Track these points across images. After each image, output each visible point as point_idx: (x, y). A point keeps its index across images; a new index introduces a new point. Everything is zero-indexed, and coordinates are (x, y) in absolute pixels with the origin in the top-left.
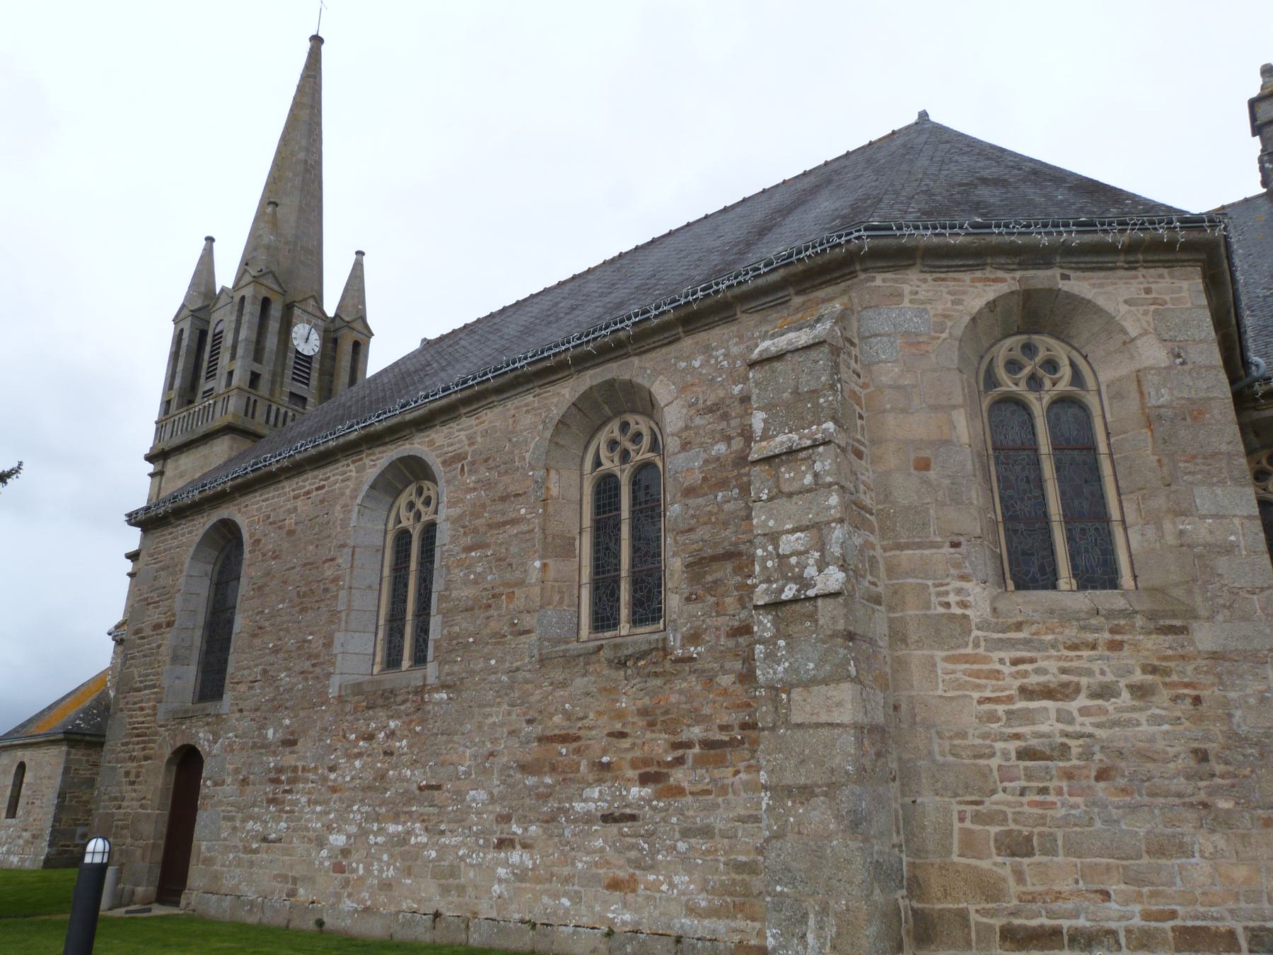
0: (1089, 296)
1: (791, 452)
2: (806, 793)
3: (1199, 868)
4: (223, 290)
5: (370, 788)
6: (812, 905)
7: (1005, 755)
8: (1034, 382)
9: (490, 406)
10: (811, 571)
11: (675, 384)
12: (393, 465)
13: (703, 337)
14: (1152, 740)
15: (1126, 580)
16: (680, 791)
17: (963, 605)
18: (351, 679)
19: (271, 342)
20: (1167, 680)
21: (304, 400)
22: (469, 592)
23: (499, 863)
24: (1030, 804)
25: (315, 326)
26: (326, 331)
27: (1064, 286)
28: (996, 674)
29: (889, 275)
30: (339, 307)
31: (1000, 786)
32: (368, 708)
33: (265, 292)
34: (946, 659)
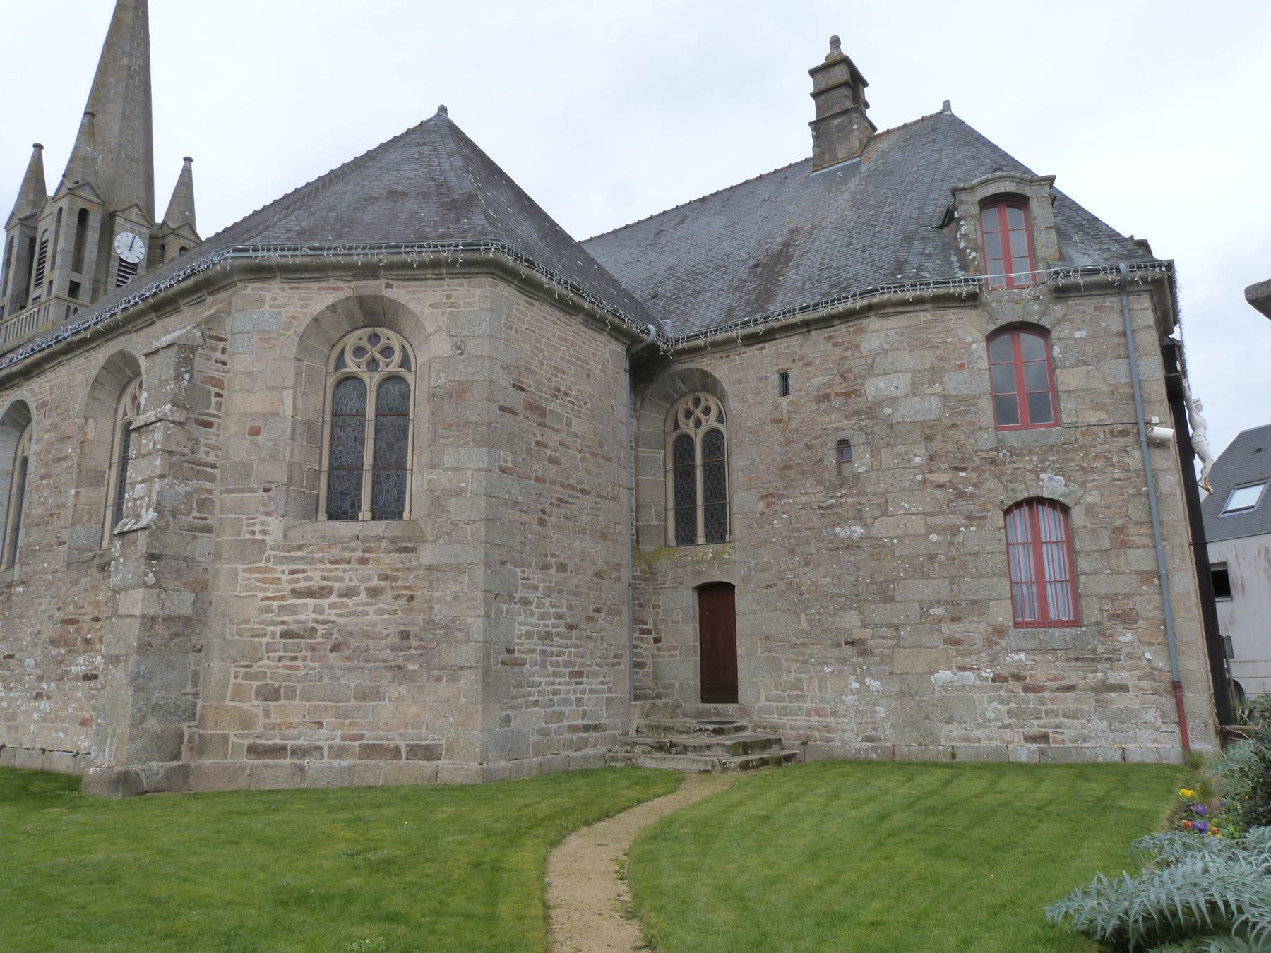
0: (403, 302)
7: (273, 635)
9: (60, 364)
14: (374, 625)
15: (406, 515)
17: (264, 533)
19: (91, 251)
20: (394, 584)
24: (285, 667)
25: (140, 235)
26: (152, 238)
27: (387, 293)
28: (277, 581)
29: (258, 285)
30: (167, 214)
31: (266, 655)
33: (81, 204)
34: (245, 570)
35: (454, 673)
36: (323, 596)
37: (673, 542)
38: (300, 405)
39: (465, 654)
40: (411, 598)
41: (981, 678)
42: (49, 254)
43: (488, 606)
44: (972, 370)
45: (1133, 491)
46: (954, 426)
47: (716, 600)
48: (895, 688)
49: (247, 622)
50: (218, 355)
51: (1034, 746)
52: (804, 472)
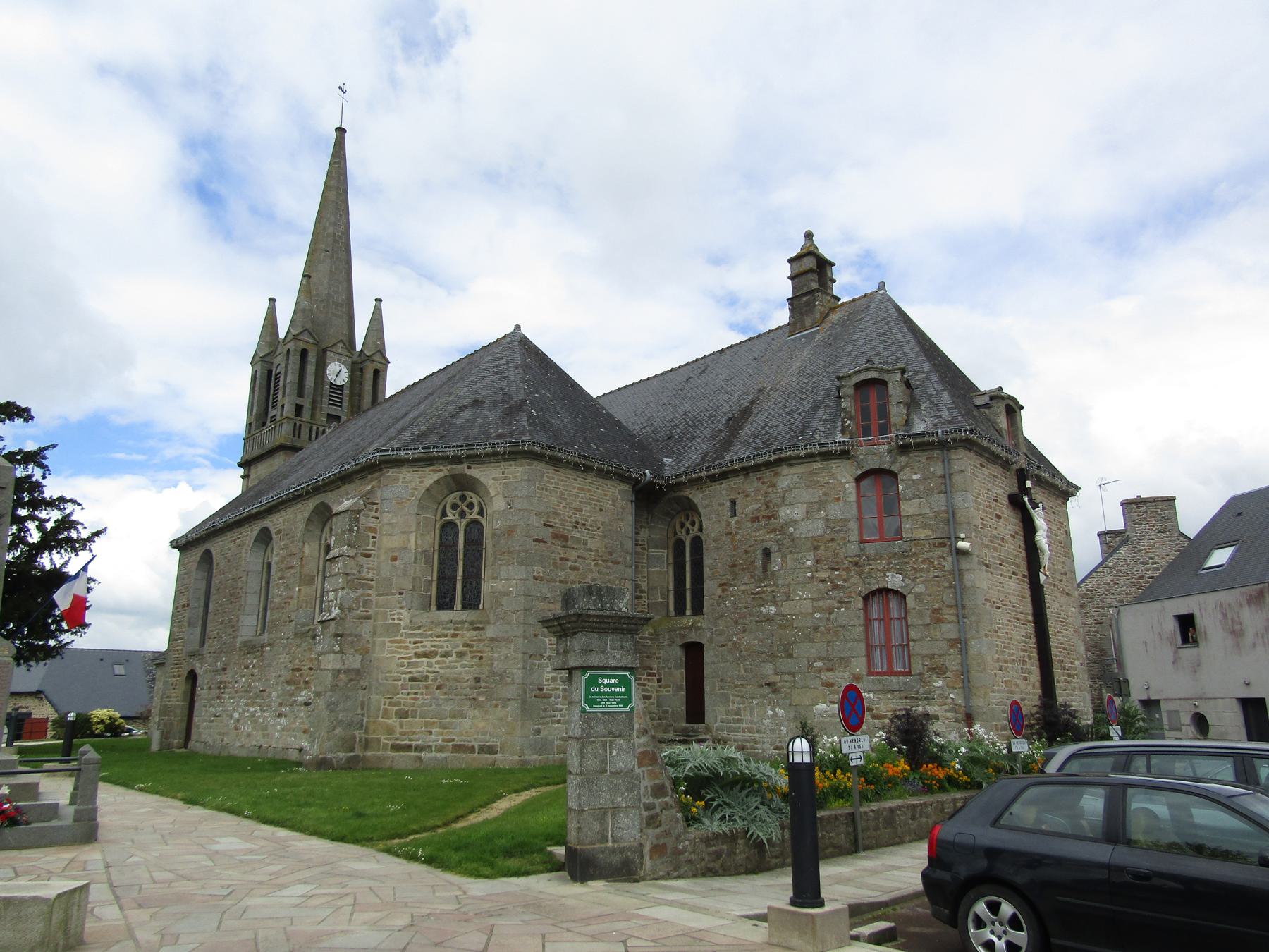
3: (467, 723)
9: (289, 507)
18: (246, 639)
27: (468, 472)
33: (302, 346)
35: (505, 702)
36: (432, 657)
37: (672, 613)
38: (419, 542)
39: (511, 691)
40: (481, 658)
42: (281, 383)
43: (525, 662)
44: (845, 502)
45: (947, 584)
46: (833, 540)
47: (694, 652)
48: (792, 715)
50: (373, 514)
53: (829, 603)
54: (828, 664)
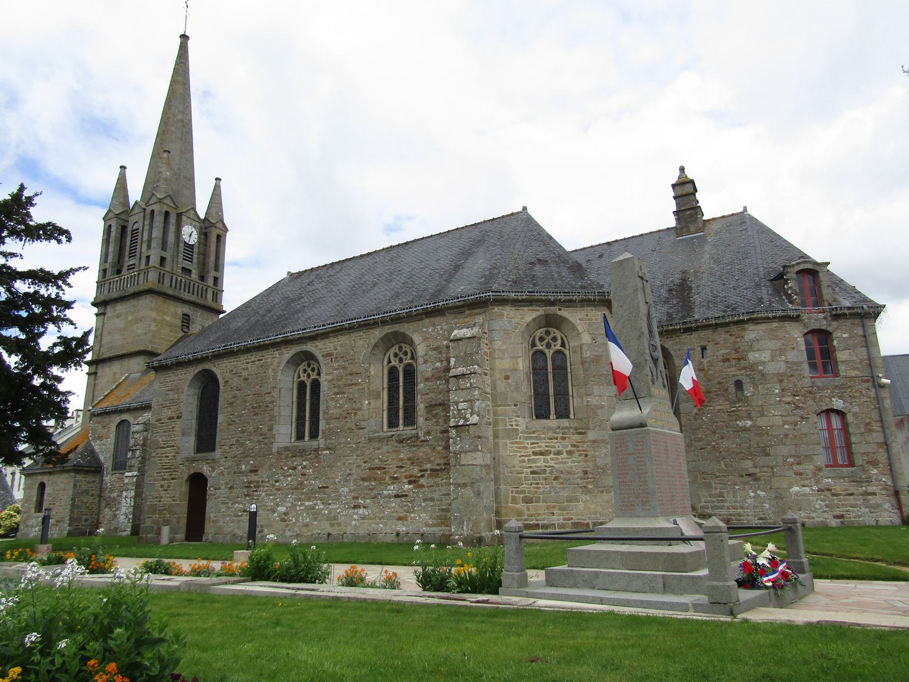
1: (463, 375)
2: (464, 485)
3: (581, 505)
4: (136, 203)
5: (296, 488)
6: (465, 518)
8: (548, 346)
9: (343, 334)
10: (468, 416)
11: (423, 338)
12: (297, 354)
13: (433, 319)
14: (571, 467)
15: (572, 416)
16: (423, 486)
17: (517, 425)
21: (189, 271)
22: (336, 412)
23: (355, 514)
27: (559, 313)
28: (526, 448)
32: (293, 457)
33: (166, 208)
41: (812, 490)
46: (792, 375)
48: (773, 495)
49: (514, 467)
51: (838, 520)
52: (718, 395)
53: (794, 418)
54: (798, 460)
